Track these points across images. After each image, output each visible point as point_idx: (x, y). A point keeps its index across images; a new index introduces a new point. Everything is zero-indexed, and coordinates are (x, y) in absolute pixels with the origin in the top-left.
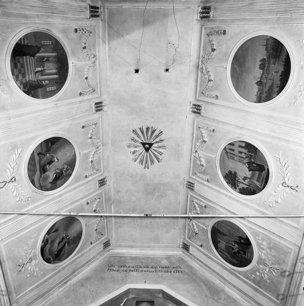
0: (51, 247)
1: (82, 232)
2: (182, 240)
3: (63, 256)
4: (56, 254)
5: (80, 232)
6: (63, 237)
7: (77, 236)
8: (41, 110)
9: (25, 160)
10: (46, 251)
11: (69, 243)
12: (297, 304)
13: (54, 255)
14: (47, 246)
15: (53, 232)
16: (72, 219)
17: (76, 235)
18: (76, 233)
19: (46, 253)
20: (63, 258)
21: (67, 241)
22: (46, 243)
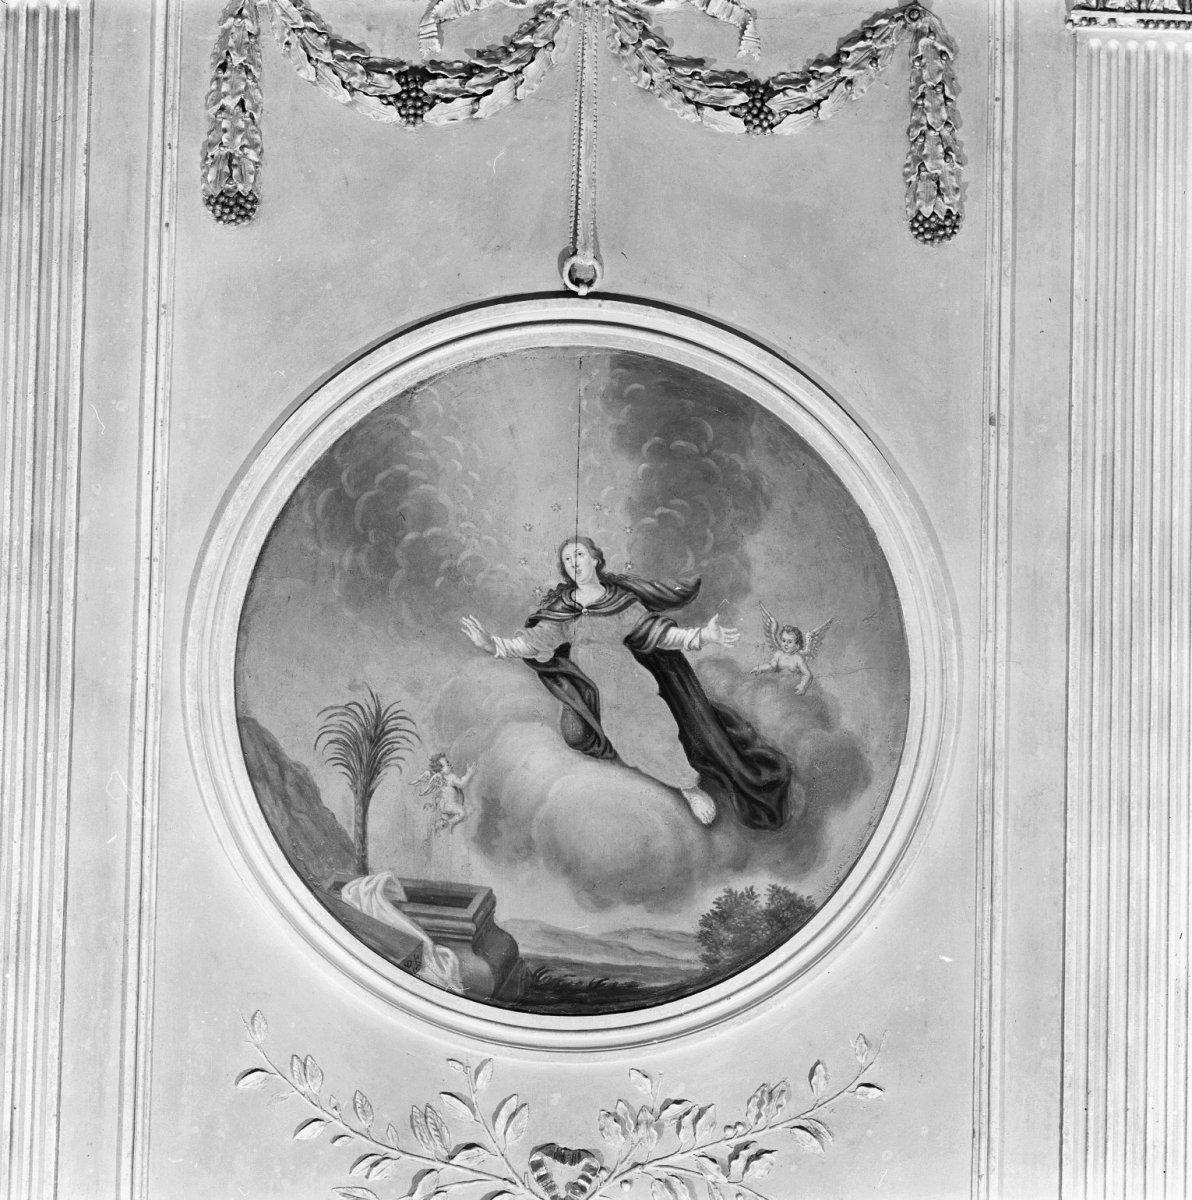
0: (568, 865)
1: (630, 363)
2: (934, 10)
3: (821, 714)
4: (720, 807)
5: (617, 396)
6: (532, 662)
7: (662, 452)
8: (38, 964)
9: (545, 1064)
10: (579, 940)
11: (684, 598)
12: (824, 446)
13: (726, 841)
14: (501, 917)
15: (365, 797)
16: (339, 495)
17: (628, 471)
18: (591, 457)
19: (606, 946)
20: (847, 723)
21: (636, 615)
22: (461, 919)
